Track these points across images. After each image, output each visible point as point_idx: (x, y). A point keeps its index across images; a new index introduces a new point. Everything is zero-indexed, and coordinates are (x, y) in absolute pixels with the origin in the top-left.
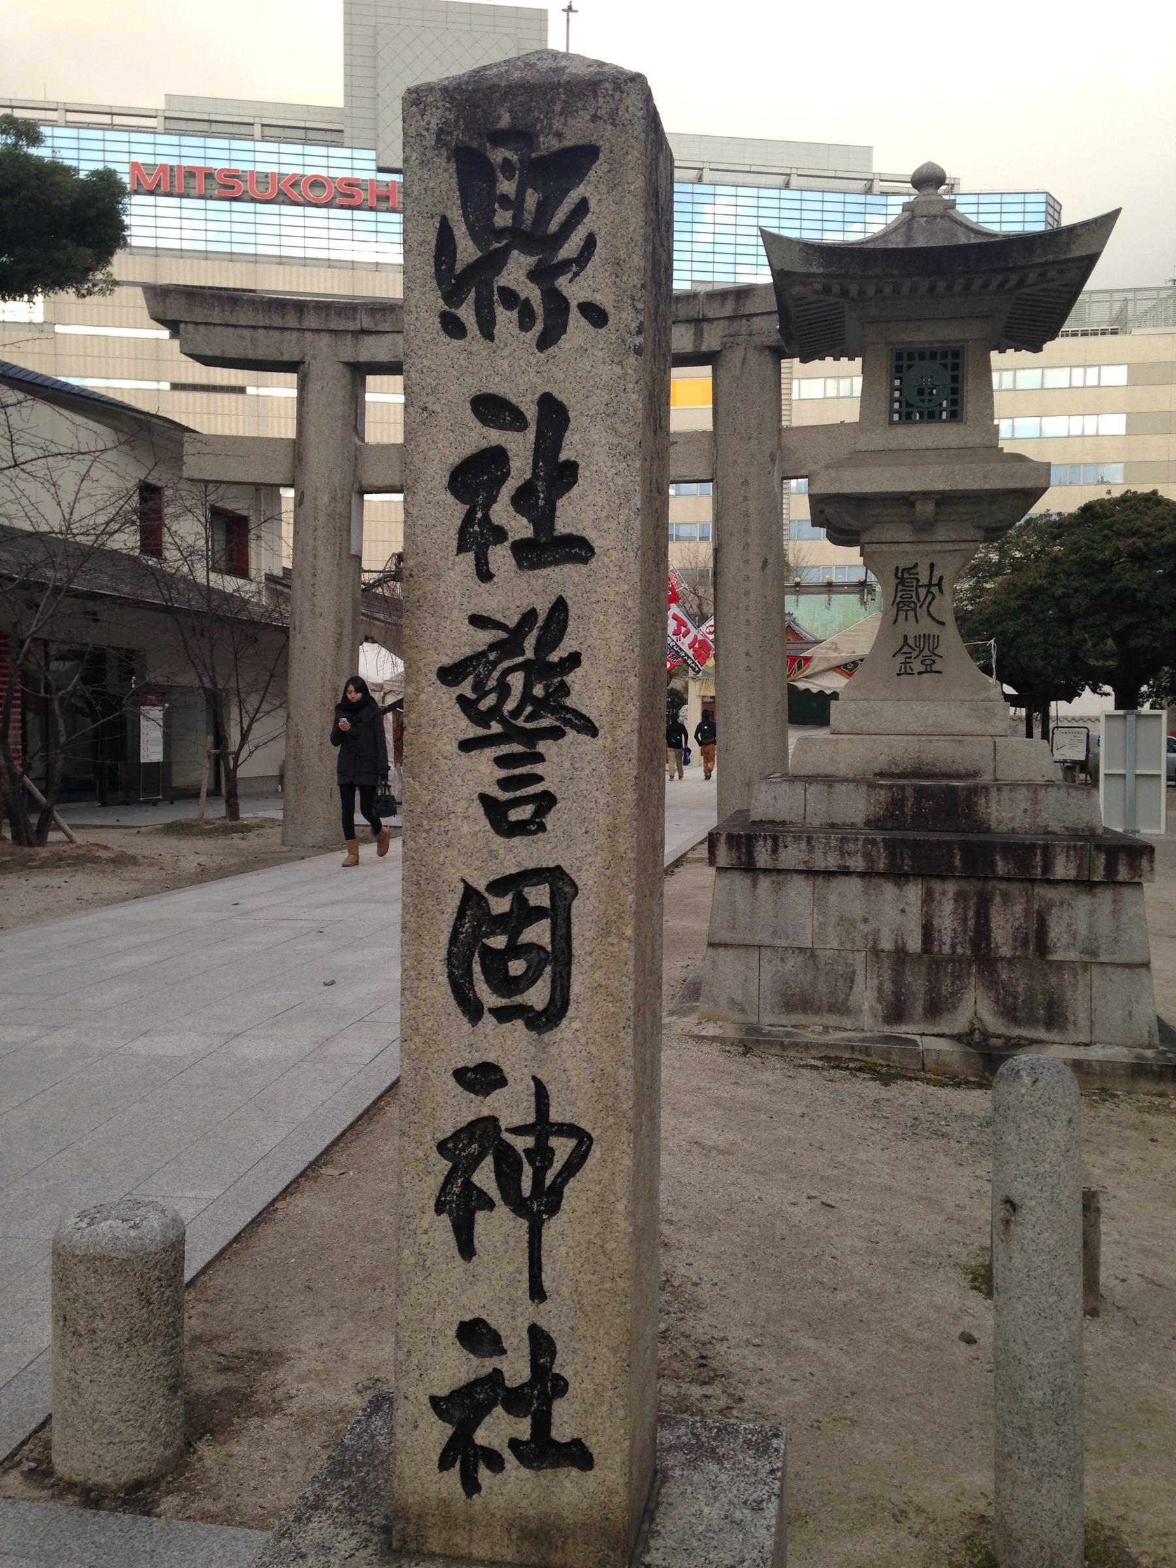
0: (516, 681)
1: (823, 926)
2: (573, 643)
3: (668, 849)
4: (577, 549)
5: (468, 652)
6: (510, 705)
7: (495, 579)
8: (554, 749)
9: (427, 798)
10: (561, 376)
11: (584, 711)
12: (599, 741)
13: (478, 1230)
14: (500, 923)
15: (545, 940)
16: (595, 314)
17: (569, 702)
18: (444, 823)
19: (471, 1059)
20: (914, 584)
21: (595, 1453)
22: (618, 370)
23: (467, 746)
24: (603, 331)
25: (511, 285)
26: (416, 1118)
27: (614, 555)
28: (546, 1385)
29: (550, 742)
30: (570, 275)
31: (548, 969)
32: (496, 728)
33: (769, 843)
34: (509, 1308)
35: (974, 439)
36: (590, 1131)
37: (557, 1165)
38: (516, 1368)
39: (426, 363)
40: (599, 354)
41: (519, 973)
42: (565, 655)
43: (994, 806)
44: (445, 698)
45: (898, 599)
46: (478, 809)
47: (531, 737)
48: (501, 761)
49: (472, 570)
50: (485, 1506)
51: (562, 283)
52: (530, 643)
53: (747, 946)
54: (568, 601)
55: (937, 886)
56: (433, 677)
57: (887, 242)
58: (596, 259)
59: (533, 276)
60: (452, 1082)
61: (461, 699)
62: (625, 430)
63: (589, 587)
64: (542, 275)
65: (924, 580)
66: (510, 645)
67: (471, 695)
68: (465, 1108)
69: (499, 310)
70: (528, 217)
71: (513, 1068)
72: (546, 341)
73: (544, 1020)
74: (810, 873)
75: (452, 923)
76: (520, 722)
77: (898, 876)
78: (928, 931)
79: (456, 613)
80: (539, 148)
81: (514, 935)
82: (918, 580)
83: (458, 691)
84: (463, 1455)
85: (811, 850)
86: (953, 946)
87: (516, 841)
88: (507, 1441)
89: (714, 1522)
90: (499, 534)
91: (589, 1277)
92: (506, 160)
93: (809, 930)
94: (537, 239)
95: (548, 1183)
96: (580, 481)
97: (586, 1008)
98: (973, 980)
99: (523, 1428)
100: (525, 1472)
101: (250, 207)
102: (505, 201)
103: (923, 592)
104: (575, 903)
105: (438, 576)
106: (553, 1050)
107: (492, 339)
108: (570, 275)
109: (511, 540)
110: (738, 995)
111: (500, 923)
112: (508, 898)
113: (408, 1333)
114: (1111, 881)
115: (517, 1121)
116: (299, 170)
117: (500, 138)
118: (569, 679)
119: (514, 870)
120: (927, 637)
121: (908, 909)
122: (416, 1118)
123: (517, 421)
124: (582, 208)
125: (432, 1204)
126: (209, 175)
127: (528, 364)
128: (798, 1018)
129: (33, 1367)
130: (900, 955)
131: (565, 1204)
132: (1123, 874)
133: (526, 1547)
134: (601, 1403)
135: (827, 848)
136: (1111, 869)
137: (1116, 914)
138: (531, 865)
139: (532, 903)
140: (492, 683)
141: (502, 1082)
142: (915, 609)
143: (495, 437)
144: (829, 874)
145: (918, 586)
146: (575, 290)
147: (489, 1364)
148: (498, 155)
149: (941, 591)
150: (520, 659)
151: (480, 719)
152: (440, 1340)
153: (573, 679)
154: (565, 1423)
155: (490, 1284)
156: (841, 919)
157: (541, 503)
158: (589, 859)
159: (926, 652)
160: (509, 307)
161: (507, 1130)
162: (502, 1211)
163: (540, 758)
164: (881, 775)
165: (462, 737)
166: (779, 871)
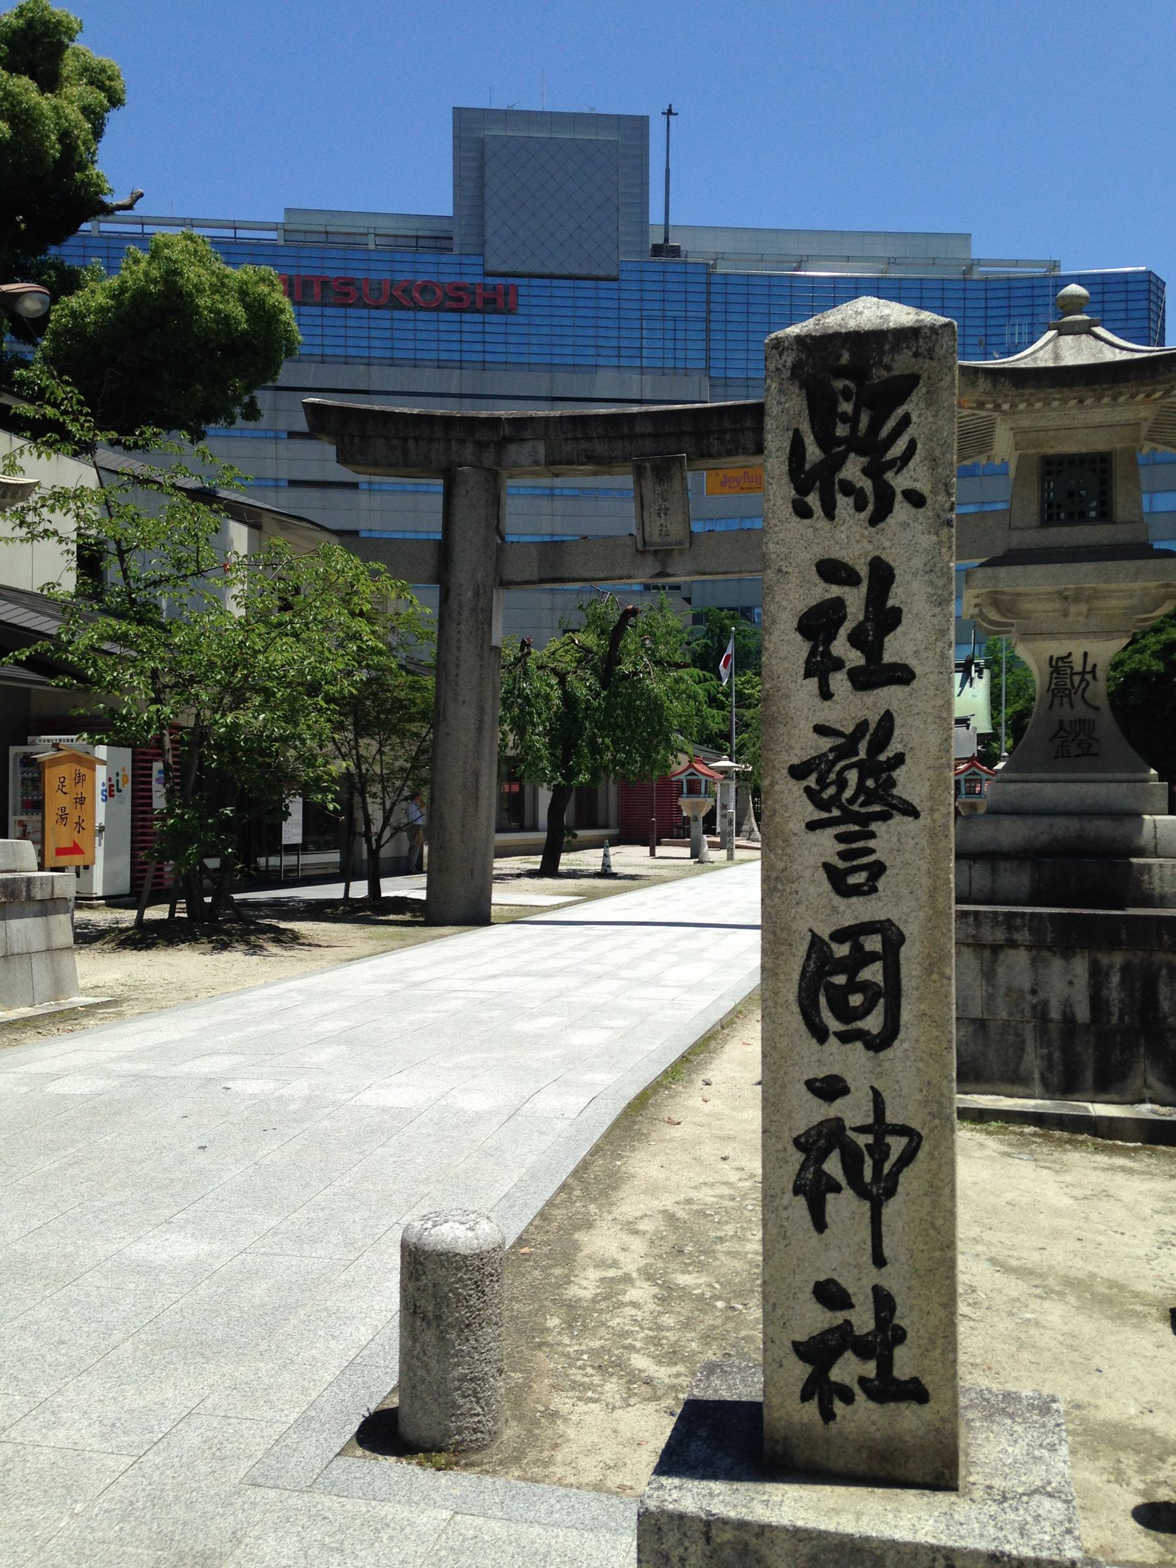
1: (991, 997)
2: (899, 746)
4: (902, 675)
6: (848, 794)
7: (835, 698)
10: (887, 544)
14: (842, 966)
15: (879, 979)
16: (916, 499)
18: (794, 886)
20: (1069, 671)
22: (934, 538)
23: (812, 826)
24: (922, 510)
25: (850, 477)
26: (776, 1118)
29: (879, 823)
30: (895, 469)
31: (882, 1000)
32: (836, 812)
34: (856, 1271)
36: (919, 1130)
38: (863, 1319)
39: (781, 536)
41: (857, 1004)
42: (891, 754)
44: (795, 788)
45: (1053, 686)
46: (822, 875)
48: (840, 838)
49: (816, 691)
51: (889, 476)
52: (863, 747)
54: (895, 714)
56: (785, 772)
57: (1035, 360)
58: (916, 459)
60: (804, 1089)
61: (808, 790)
63: (911, 702)
64: (874, 471)
66: (846, 749)
67: (813, 785)
68: (817, 1111)
71: (854, 1078)
72: (876, 520)
73: (880, 1043)
75: (802, 963)
76: (855, 808)
78: (1097, 1002)
80: (872, 378)
81: (852, 975)
82: (1072, 668)
83: (805, 783)
86: (1121, 1018)
88: (856, 1378)
89: (1019, 1457)
90: (838, 664)
91: (922, 1247)
92: (845, 387)
93: (978, 1001)
94: (873, 449)
98: (1142, 1050)
100: (872, 1405)
101: (364, 313)
102: (844, 418)
104: (903, 949)
105: (788, 697)
108: (895, 469)
109: (845, 670)
113: (774, 1289)
115: (859, 1122)
116: (410, 277)
117: (840, 373)
118: (895, 774)
120: (1082, 722)
121: (1076, 981)
122: (776, 1118)
124: (906, 421)
125: (791, 1186)
126: (325, 283)
129: (359, 1360)
131: (900, 1189)
134: (935, 1349)
140: (833, 776)
141: (845, 1091)
142: (1069, 696)
143: (835, 591)
144: (996, 949)
145: (1072, 674)
146: (900, 482)
147: (839, 1317)
148: (839, 384)
149: (1095, 678)
150: (855, 759)
152: (800, 1295)
153: (899, 774)
154: (905, 1363)
156: (1010, 990)
157: (870, 638)
158: (915, 914)
159: (1082, 736)
161: (851, 1129)
162: (848, 1193)
163: (872, 835)
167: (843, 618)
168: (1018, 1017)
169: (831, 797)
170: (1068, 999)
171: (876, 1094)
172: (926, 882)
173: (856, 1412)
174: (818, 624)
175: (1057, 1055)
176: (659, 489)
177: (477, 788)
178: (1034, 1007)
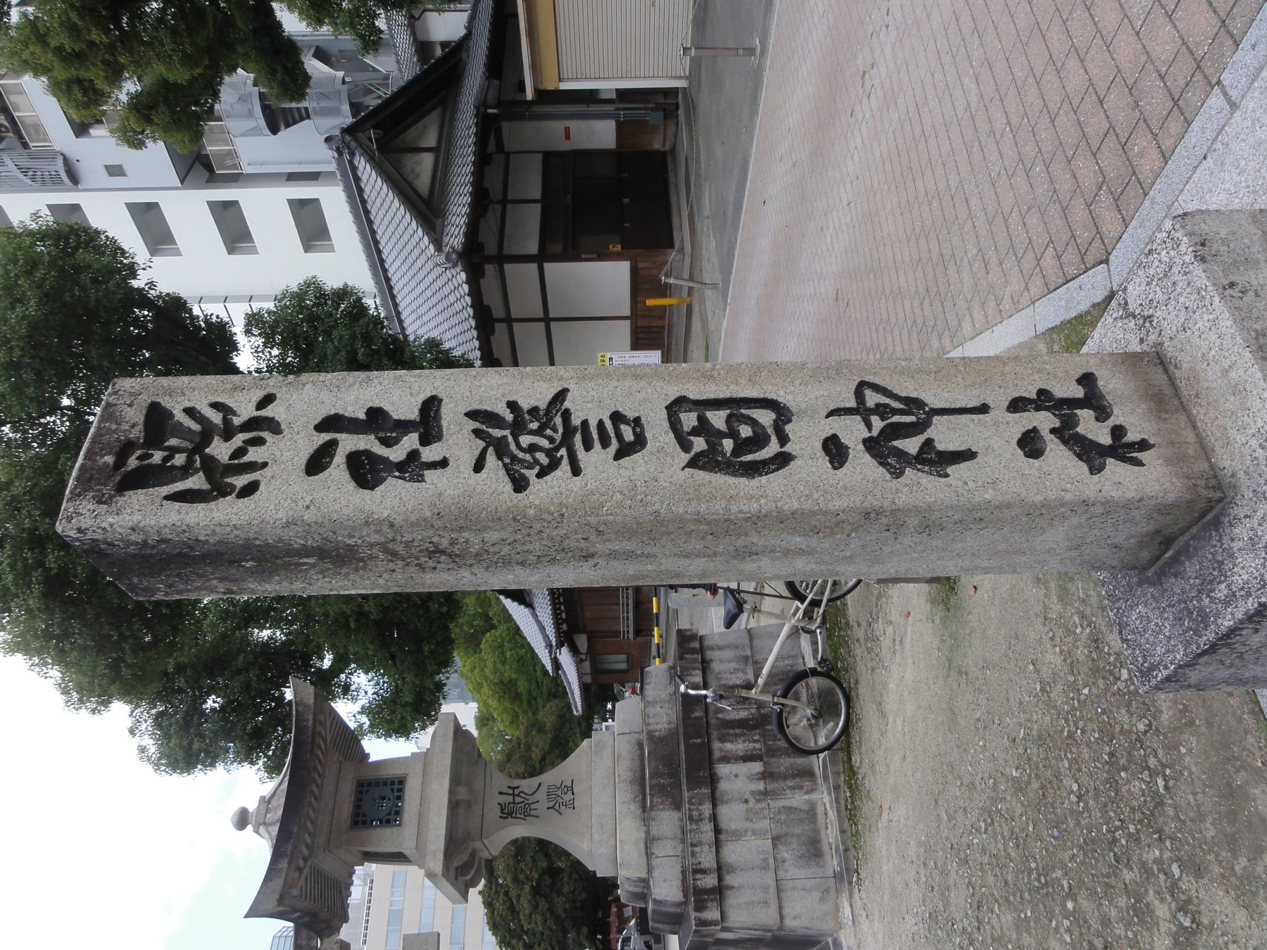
0: (526, 440)
1: (754, 832)
4: (431, 406)
6: (545, 443)
19: (825, 462)
22: (308, 386)
23: (576, 471)
33: (698, 876)
35: (418, 768)
37: (887, 401)
38: (1045, 421)
43: (659, 726)
46: (625, 461)
48: (588, 446)
51: (237, 421)
52: (497, 433)
53: (779, 891)
55: (717, 754)
56: (521, 496)
61: (539, 476)
62: (352, 380)
64: (228, 434)
65: (510, 799)
66: (501, 449)
67: (537, 469)
68: (862, 465)
69: (246, 459)
73: (783, 414)
74: (718, 844)
76: (558, 437)
77: (713, 780)
78: (748, 758)
79: (470, 482)
85: (700, 844)
86: (755, 741)
90: (413, 455)
93: (759, 842)
95: (902, 406)
96: (381, 405)
103: (518, 799)
106: (803, 406)
109: (421, 449)
110: (816, 895)
111: (714, 448)
114: (702, 650)
115: (862, 426)
119: (671, 435)
124: (190, 412)
127: (290, 439)
128: (825, 848)
130: (766, 775)
131: (914, 395)
132: (696, 645)
135: (697, 831)
136: (694, 651)
137: (720, 648)
138: (667, 424)
140: (528, 457)
143: (340, 459)
144: (717, 831)
150: (510, 438)
151: (554, 464)
153: (525, 404)
159: (559, 793)
162: (930, 433)
163: (585, 424)
164: (644, 807)
165: (570, 474)
166: (719, 869)
167: (368, 453)
168: (766, 812)
169: (547, 455)
170: (749, 778)
171: (831, 414)
172: (628, 382)
173: (1131, 424)
174: (366, 471)
175: (790, 783)
178: (758, 801)
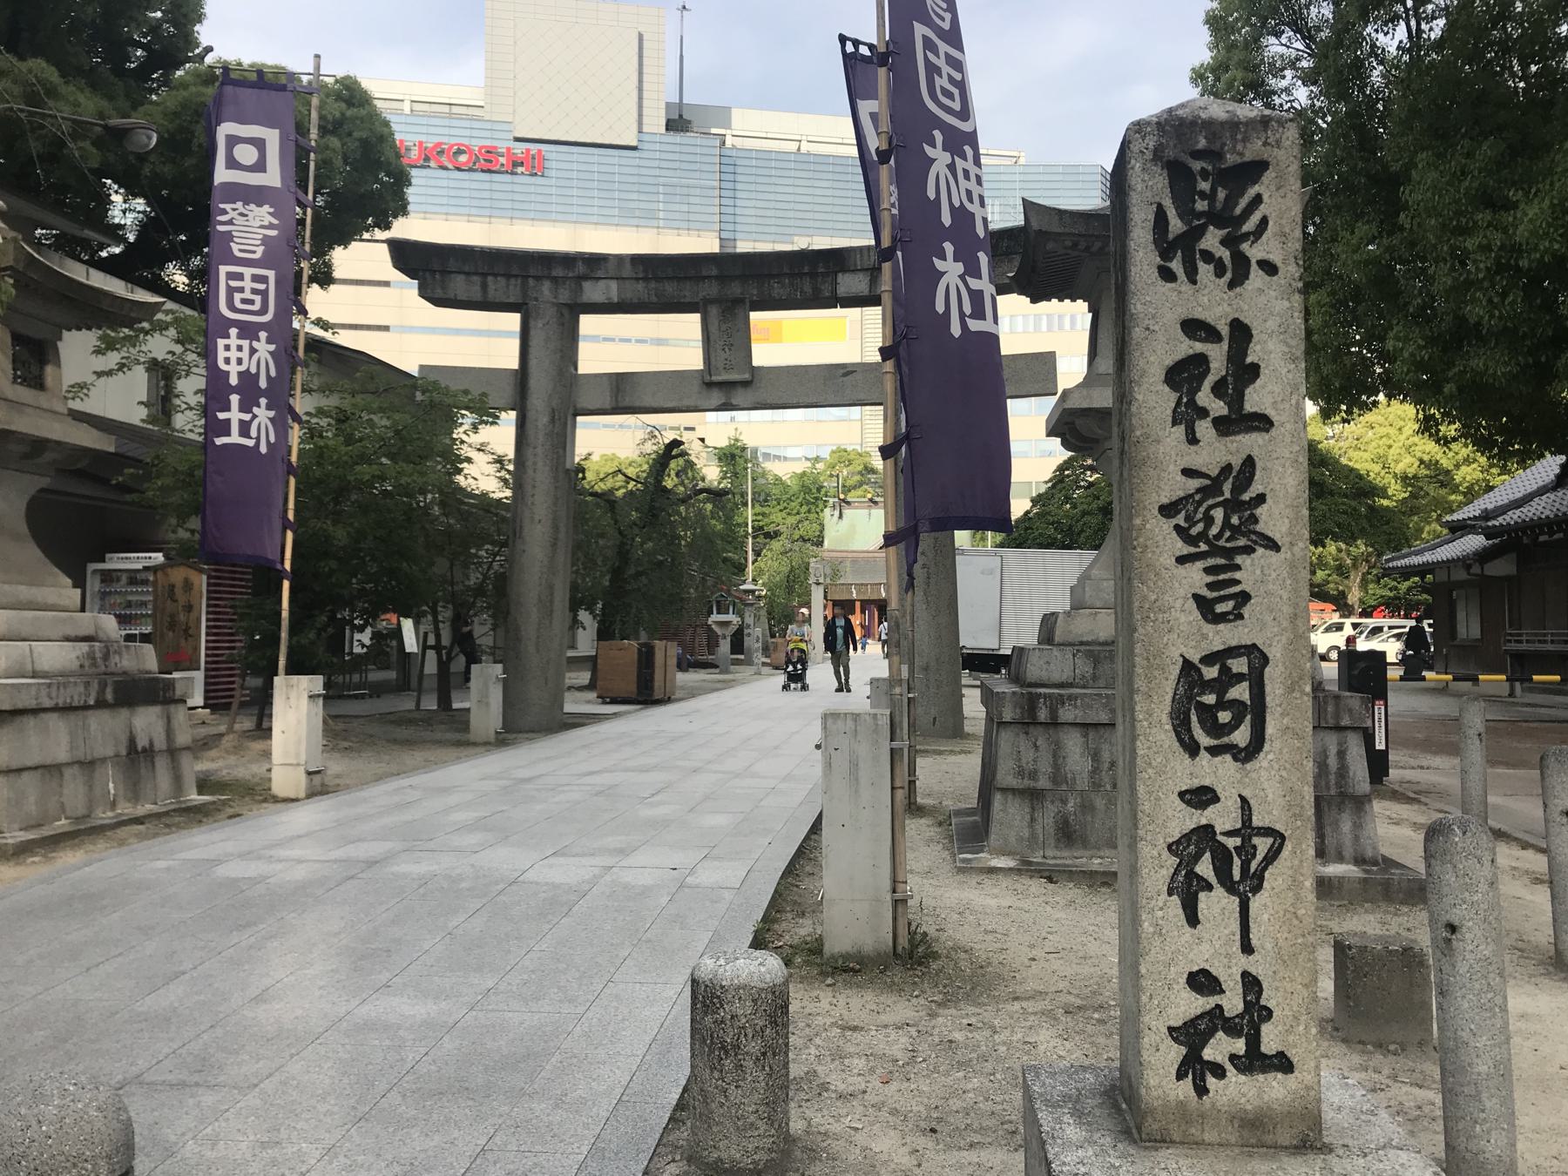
0: (1218, 514)
3: (577, 451)
4: (1262, 422)
5: (1181, 494)
6: (1214, 531)
8: (1248, 561)
9: (1153, 597)
11: (1270, 534)
12: (1282, 555)
13: (1201, 906)
15: (1246, 697)
16: (1269, 268)
17: (1259, 528)
21: (1295, 1061)
22: (1287, 304)
23: (1181, 560)
27: (1288, 426)
28: (1257, 1012)
32: (1203, 547)
37: (1259, 857)
38: (1233, 1003)
40: (1273, 293)
44: (1165, 527)
47: (1229, 553)
48: (1208, 571)
49: (1183, 437)
50: (1213, 1105)
51: (1245, 247)
59: (1223, 242)
60: (1178, 801)
61: (1177, 528)
62: (1294, 343)
64: (1230, 242)
67: (1183, 524)
70: (1219, 206)
76: (1222, 543)
79: (1172, 467)
81: (1221, 694)
83: (1174, 521)
84: (1195, 1068)
87: (1221, 626)
90: (1203, 413)
97: (1277, 744)
99: (1240, 1046)
100: (1242, 1078)
102: (1203, 195)
107: (1194, 282)
111: (1207, 686)
112: (1217, 667)
115: (1228, 827)
117: (1197, 155)
118: (1258, 512)
119: (1221, 647)
123: (1212, 334)
124: (1258, 199)
131: (1265, 884)
133: (1246, 1133)
138: (1234, 643)
139: (1235, 671)
140: (1199, 516)
141: (1216, 799)
143: (1199, 347)
147: (1212, 1001)
148: (1197, 166)
153: (1261, 511)
155: (1212, 942)
160: (1207, 262)
161: (1224, 834)
162: (1219, 891)
163: (1238, 568)
165: (1178, 554)
176: (724, 327)
177: (551, 602)
